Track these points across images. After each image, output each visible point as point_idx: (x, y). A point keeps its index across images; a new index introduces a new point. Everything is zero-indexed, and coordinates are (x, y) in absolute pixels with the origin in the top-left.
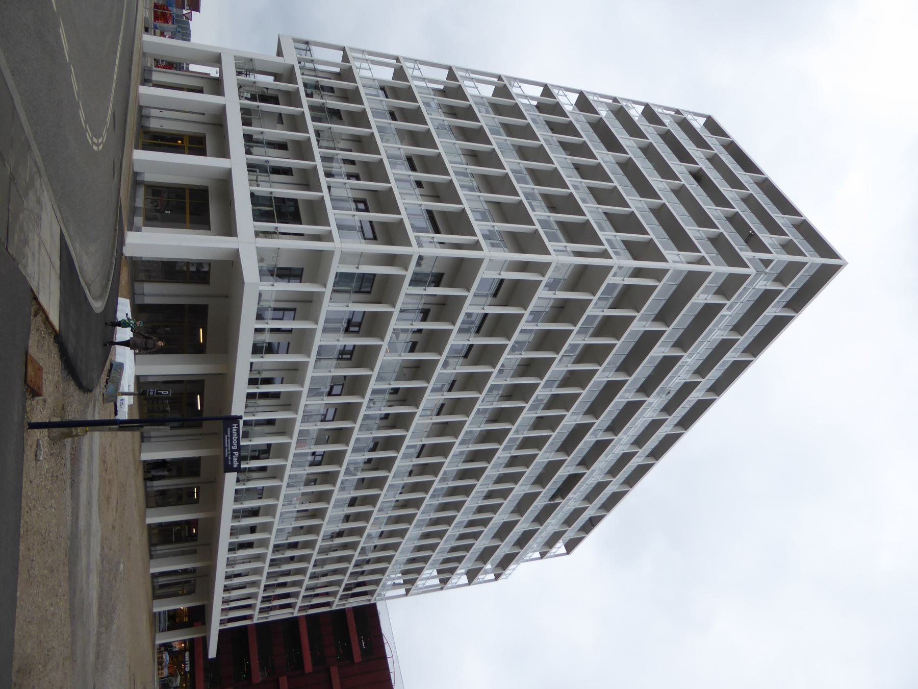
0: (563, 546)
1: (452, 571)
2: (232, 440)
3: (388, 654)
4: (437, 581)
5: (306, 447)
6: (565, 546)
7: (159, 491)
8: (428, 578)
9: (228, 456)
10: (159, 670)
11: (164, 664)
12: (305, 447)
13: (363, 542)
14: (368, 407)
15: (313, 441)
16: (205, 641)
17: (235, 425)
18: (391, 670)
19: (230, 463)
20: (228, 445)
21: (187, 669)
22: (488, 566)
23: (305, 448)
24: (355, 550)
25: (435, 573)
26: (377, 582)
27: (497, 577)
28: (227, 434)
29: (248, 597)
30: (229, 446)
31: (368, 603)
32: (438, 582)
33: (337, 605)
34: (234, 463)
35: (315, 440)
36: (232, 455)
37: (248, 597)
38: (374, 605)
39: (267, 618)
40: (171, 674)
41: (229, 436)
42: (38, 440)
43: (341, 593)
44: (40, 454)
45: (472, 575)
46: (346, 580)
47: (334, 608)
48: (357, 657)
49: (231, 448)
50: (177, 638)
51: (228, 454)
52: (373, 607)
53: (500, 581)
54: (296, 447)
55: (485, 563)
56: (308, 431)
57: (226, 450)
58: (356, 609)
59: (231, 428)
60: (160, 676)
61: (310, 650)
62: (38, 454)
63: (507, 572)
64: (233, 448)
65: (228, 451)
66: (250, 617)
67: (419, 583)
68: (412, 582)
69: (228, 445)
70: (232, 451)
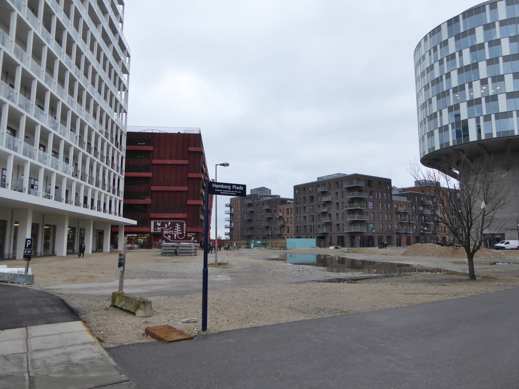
0: (119, 5)
1: (120, 81)
2: (224, 189)
3: (150, 131)
4: (123, 92)
5: (35, 152)
6: (120, 4)
7: (44, 250)
8: (121, 97)
9: (235, 193)
10: (134, 249)
11: (132, 247)
12: (34, 153)
13: (96, 130)
14: (13, 101)
15: (32, 147)
16: (127, 226)
17: (213, 185)
18: (159, 132)
19: (240, 192)
20: (227, 192)
21: (136, 235)
22: (122, 58)
23: (35, 153)
24: (100, 136)
25: (119, 92)
26: (117, 128)
27: (128, 56)
28: (220, 192)
29: (116, 201)
30: (228, 191)
31: (126, 135)
32: (124, 92)
33: (124, 154)
34: (240, 189)
35: (31, 145)
36: (234, 189)
37: (116, 201)
38: (127, 132)
39: (122, 193)
40: (137, 243)
41: (221, 191)
42: (183, 322)
43: (118, 150)
44: (194, 320)
45: (125, 71)
46: (113, 145)
47: (124, 155)
48: (150, 148)
49: (229, 190)
50: (122, 240)
51: (234, 193)
52: (129, 134)
53: (131, 55)
54: (34, 159)
55: (120, 59)
56: (24, 149)
57: (231, 194)
58: (128, 144)
59: (215, 188)
60: (137, 248)
61: (141, 172)
62: (194, 321)
63: (127, 47)
64: (230, 188)
65: (231, 192)
66: (120, 201)
67: (123, 103)
68: (121, 107)
69: (227, 192)
70: (231, 189)
